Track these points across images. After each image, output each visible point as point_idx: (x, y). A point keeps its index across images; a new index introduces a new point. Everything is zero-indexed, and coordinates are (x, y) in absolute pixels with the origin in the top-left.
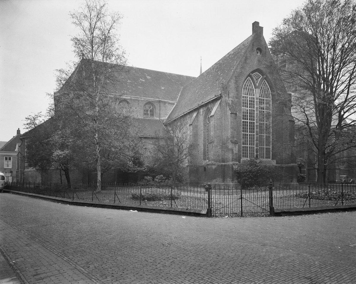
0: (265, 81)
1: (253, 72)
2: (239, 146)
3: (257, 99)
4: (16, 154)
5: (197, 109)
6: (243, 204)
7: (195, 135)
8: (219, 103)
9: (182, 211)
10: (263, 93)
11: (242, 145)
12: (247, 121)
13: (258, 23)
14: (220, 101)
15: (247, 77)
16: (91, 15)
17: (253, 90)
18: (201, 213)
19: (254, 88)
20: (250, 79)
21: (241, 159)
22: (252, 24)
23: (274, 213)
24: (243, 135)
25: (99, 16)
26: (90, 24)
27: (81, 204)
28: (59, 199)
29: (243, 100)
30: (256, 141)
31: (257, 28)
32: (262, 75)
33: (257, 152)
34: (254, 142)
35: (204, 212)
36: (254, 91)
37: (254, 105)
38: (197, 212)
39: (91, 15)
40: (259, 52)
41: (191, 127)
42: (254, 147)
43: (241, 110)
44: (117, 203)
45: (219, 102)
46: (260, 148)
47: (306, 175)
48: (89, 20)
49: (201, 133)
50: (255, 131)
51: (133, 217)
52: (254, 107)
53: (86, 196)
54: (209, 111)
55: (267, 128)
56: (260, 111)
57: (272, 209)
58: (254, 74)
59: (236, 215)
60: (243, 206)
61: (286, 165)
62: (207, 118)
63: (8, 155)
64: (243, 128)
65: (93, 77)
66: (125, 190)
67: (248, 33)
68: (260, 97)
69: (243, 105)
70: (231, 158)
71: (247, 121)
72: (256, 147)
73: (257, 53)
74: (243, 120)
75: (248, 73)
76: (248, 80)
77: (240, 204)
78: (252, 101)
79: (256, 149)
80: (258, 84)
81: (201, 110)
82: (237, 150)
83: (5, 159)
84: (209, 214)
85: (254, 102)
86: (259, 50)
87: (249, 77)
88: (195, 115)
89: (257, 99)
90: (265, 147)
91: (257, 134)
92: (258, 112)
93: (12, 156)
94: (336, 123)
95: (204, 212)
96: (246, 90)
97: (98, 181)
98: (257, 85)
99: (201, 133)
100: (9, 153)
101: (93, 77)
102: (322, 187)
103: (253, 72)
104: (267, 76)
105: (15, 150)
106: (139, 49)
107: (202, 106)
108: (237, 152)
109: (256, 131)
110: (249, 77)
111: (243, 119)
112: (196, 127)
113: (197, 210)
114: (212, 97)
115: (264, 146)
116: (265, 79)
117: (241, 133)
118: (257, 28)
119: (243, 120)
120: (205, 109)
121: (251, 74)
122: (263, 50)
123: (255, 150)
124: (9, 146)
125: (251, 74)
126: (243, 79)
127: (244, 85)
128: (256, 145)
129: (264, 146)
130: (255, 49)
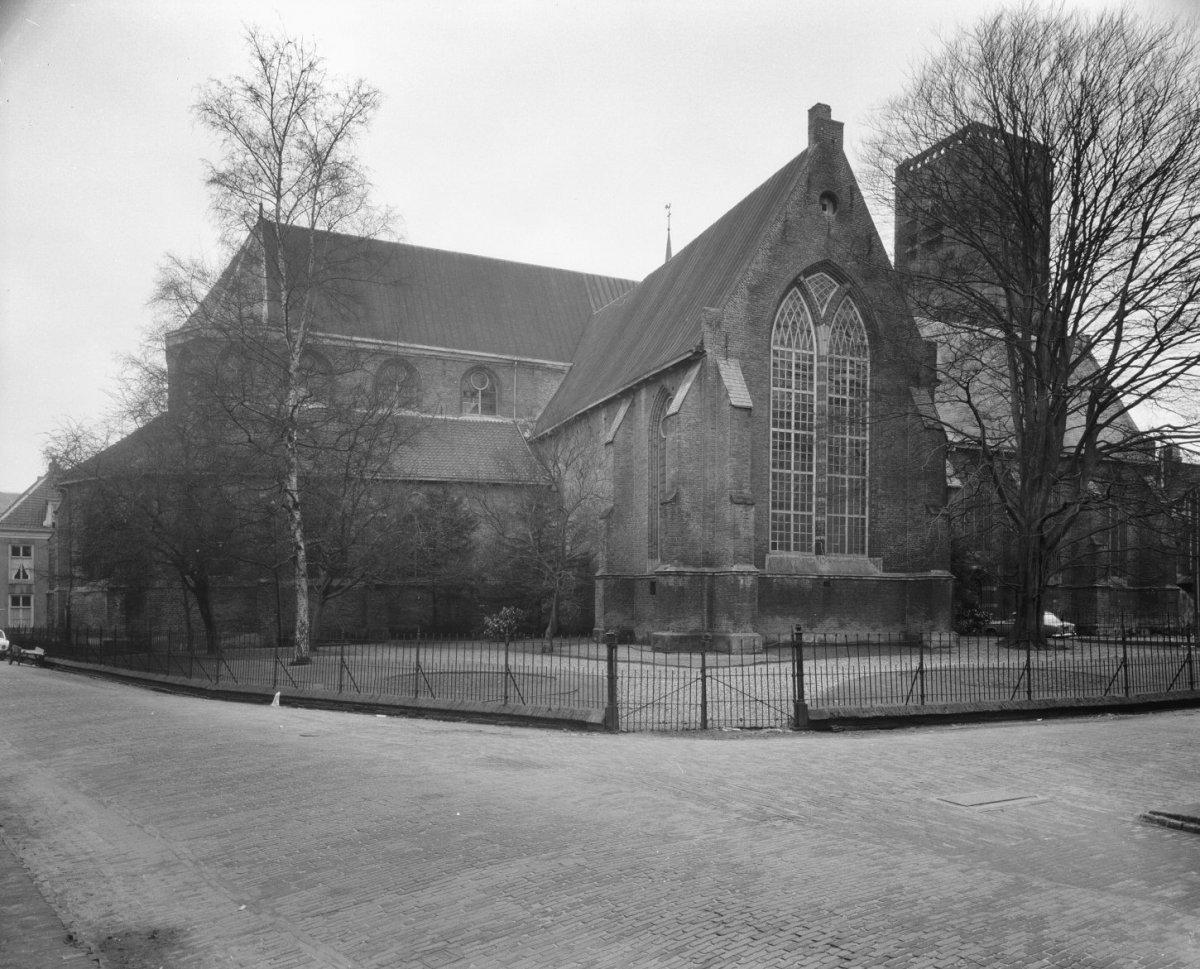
0: (848, 302)
1: (807, 272)
2: (758, 514)
3: (821, 359)
4: (46, 537)
5: (630, 393)
6: (700, 690)
7: (624, 479)
8: (696, 373)
9: (534, 715)
10: (840, 339)
11: (771, 511)
12: (788, 431)
13: (828, 109)
14: (698, 367)
15: (789, 288)
16: (273, 94)
17: (809, 332)
18: (588, 720)
19: (811, 324)
20: (799, 294)
21: (768, 557)
22: (809, 111)
23: (808, 721)
24: (774, 477)
25: (300, 102)
26: (272, 122)
27: (397, 711)
28: (131, 675)
29: (775, 365)
30: (818, 496)
31: (824, 127)
32: (840, 282)
33: (819, 532)
34: (810, 499)
35: (596, 717)
36: (813, 333)
37: (811, 378)
38: (575, 718)
39: (273, 94)
40: (831, 205)
41: (611, 449)
42: (810, 517)
43: (769, 395)
44: (349, 695)
45: (694, 372)
46: (829, 518)
47: (995, 605)
48: (268, 110)
49: (642, 471)
50: (814, 466)
51: (274, 716)
52: (811, 385)
53: (259, 670)
54: (666, 396)
55: (858, 455)
56: (831, 399)
57: (800, 705)
58: (810, 278)
59: (686, 731)
60: (708, 699)
61: (918, 575)
62: (660, 418)
63: (21, 540)
64: (775, 454)
65: (302, 297)
66: (372, 654)
67: (796, 141)
68: (831, 352)
69: (775, 380)
70: (732, 551)
71: (788, 431)
72: (817, 516)
73: (824, 209)
74: (775, 430)
75: (791, 277)
76: (791, 298)
77: (700, 695)
78: (804, 366)
79: (816, 522)
80: (824, 310)
81: (643, 395)
82: (751, 525)
83: (10, 552)
84: (610, 724)
85: (811, 367)
86: (830, 197)
87: (795, 288)
88: (622, 411)
89: (821, 359)
90: (847, 516)
91: (819, 475)
92: (826, 403)
93: (33, 541)
94: (1080, 433)
95: (596, 717)
96: (786, 332)
97: (299, 624)
98: (823, 312)
99: (642, 471)
100: (13, 533)
101: (302, 297)
102: (1032, 646)
103: (807, 272)
104: (853, 283)
105: (45, 523)
106: (420, 196)
107: (647, 382)
108: (752, 534)
109: (817, 464)
110: (795, 288)
111: (775, 425)
112: (627, 450)
113: (578, 711)
114: (668, 358)
115: (844, 512)
116: (849, 293)
117: (769, 471)
118: (824, 127)
119: (775, 430)
120: (656, 390)
121: (802, 278)
122: (844, 197)
123: (814, 527)
124: (29, 509)
125: (802, 278)
126: (777, 294)
127: (778, 315)
128: (817, 511)
129: (843, 512)
130: (816, 195)
